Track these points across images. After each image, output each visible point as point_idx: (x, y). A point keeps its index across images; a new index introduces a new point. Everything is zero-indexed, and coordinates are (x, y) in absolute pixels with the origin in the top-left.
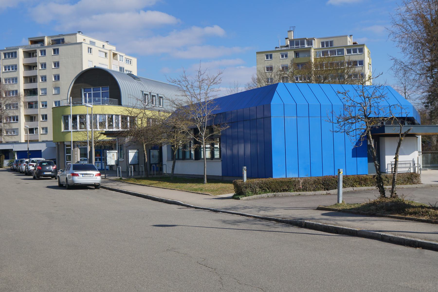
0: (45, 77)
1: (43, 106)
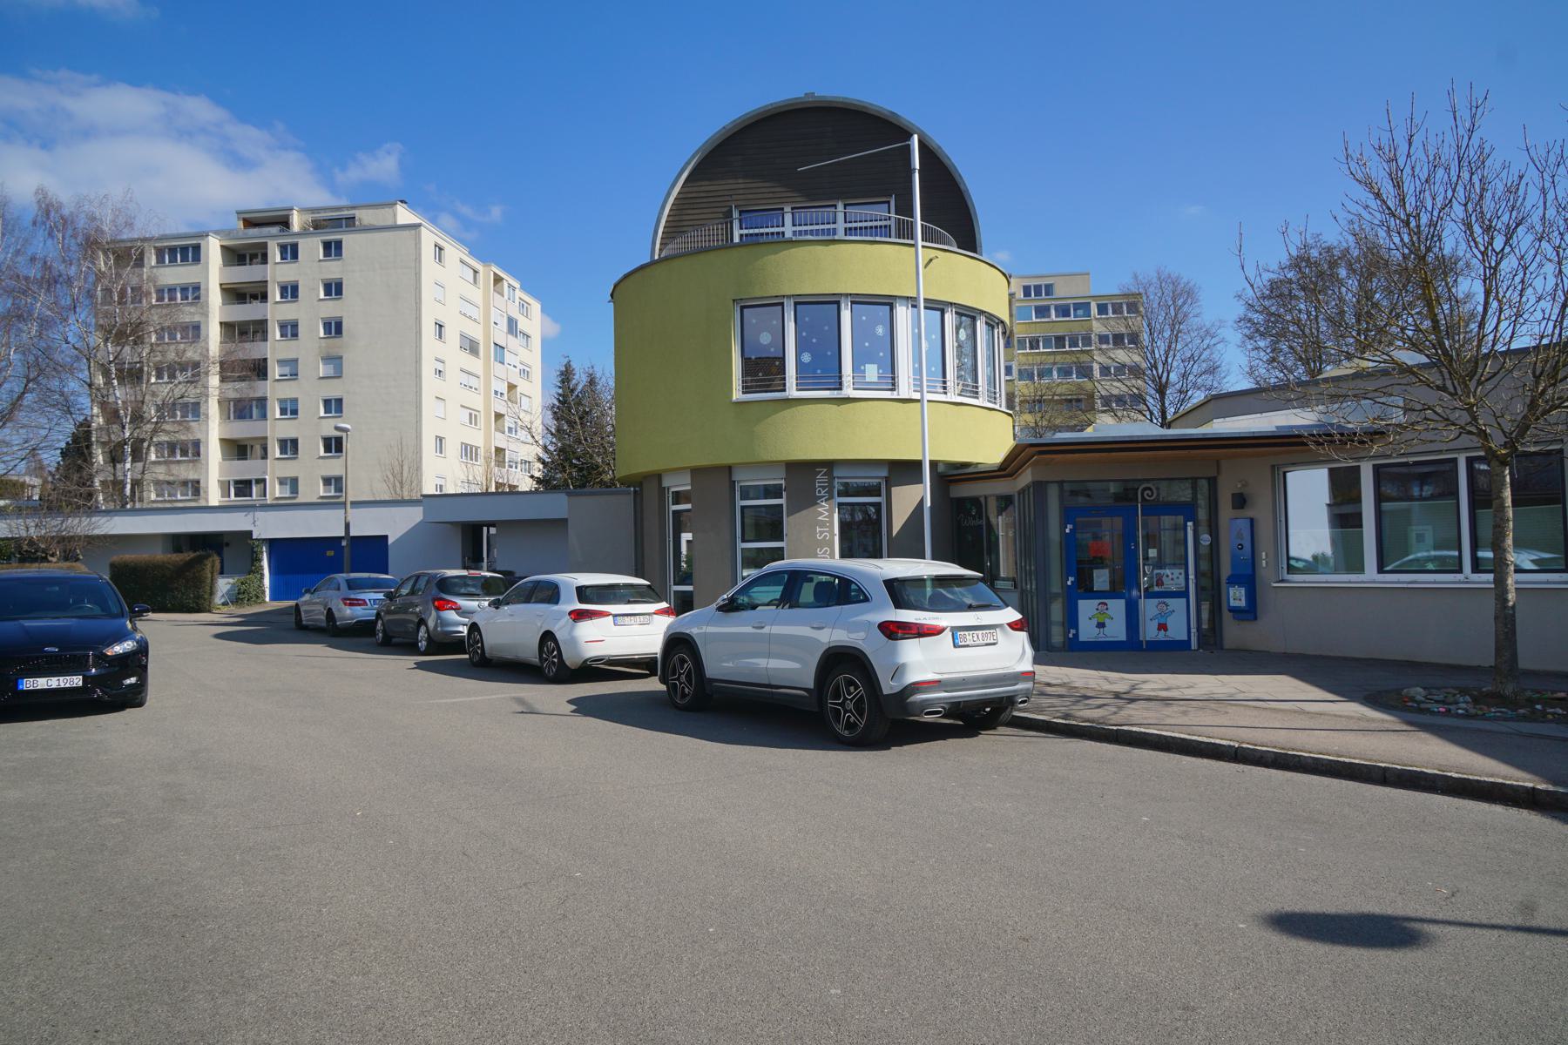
0: (295, 325)
1: (283, 411)
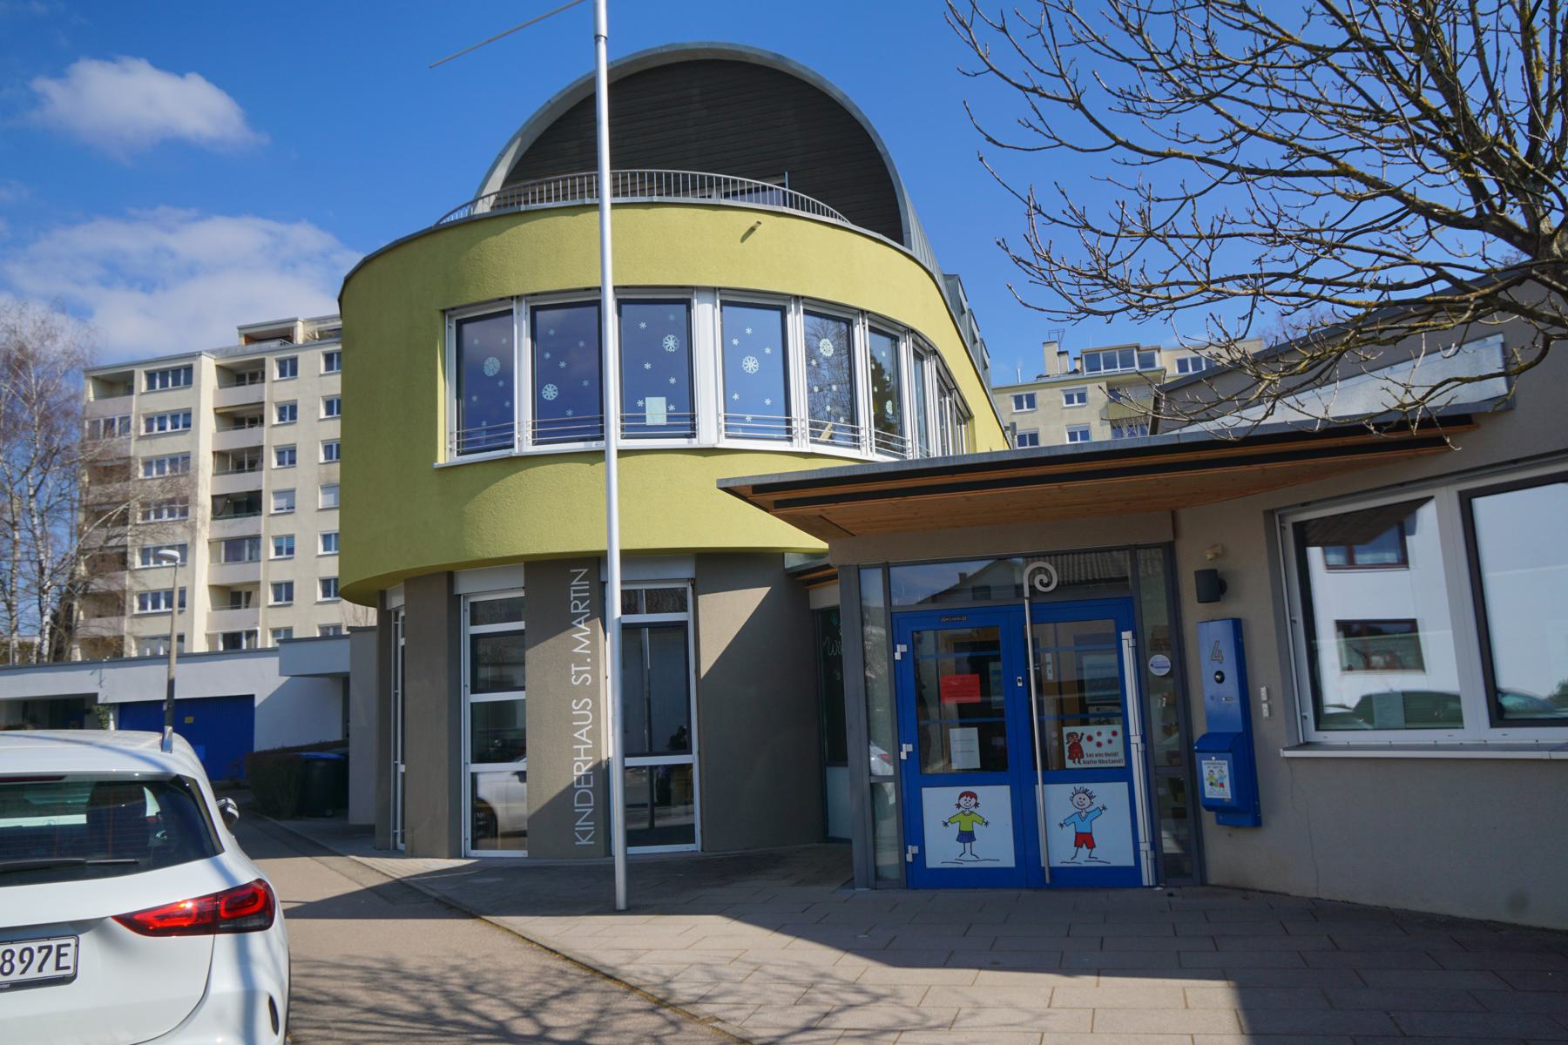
1: (279, 551)
